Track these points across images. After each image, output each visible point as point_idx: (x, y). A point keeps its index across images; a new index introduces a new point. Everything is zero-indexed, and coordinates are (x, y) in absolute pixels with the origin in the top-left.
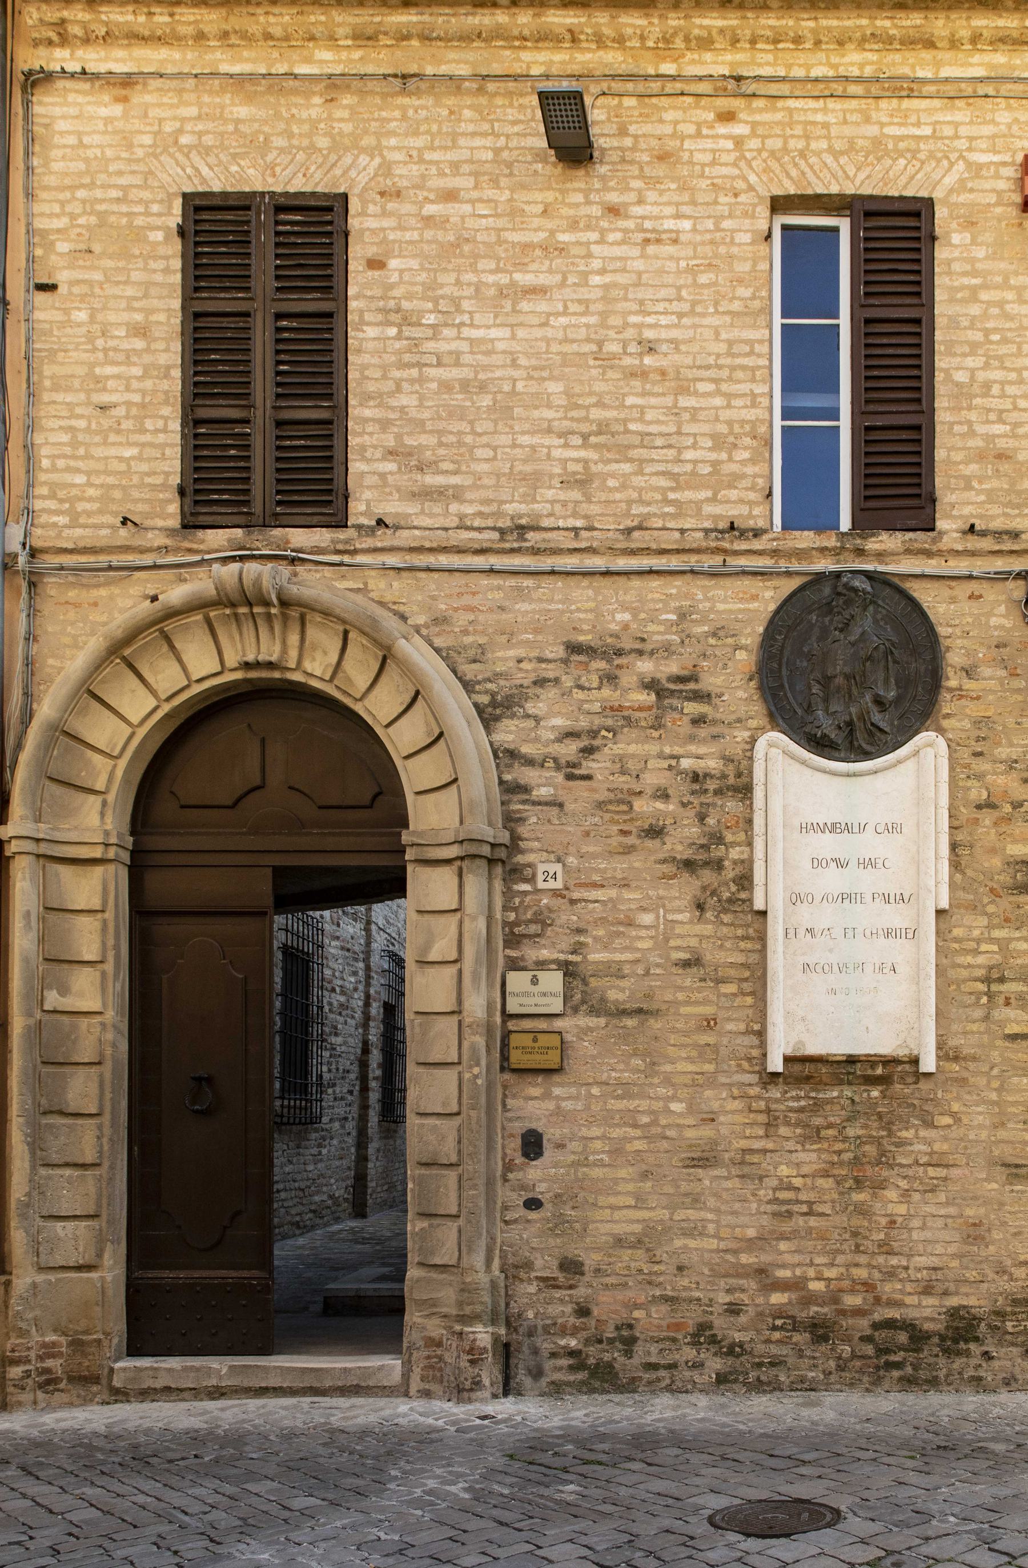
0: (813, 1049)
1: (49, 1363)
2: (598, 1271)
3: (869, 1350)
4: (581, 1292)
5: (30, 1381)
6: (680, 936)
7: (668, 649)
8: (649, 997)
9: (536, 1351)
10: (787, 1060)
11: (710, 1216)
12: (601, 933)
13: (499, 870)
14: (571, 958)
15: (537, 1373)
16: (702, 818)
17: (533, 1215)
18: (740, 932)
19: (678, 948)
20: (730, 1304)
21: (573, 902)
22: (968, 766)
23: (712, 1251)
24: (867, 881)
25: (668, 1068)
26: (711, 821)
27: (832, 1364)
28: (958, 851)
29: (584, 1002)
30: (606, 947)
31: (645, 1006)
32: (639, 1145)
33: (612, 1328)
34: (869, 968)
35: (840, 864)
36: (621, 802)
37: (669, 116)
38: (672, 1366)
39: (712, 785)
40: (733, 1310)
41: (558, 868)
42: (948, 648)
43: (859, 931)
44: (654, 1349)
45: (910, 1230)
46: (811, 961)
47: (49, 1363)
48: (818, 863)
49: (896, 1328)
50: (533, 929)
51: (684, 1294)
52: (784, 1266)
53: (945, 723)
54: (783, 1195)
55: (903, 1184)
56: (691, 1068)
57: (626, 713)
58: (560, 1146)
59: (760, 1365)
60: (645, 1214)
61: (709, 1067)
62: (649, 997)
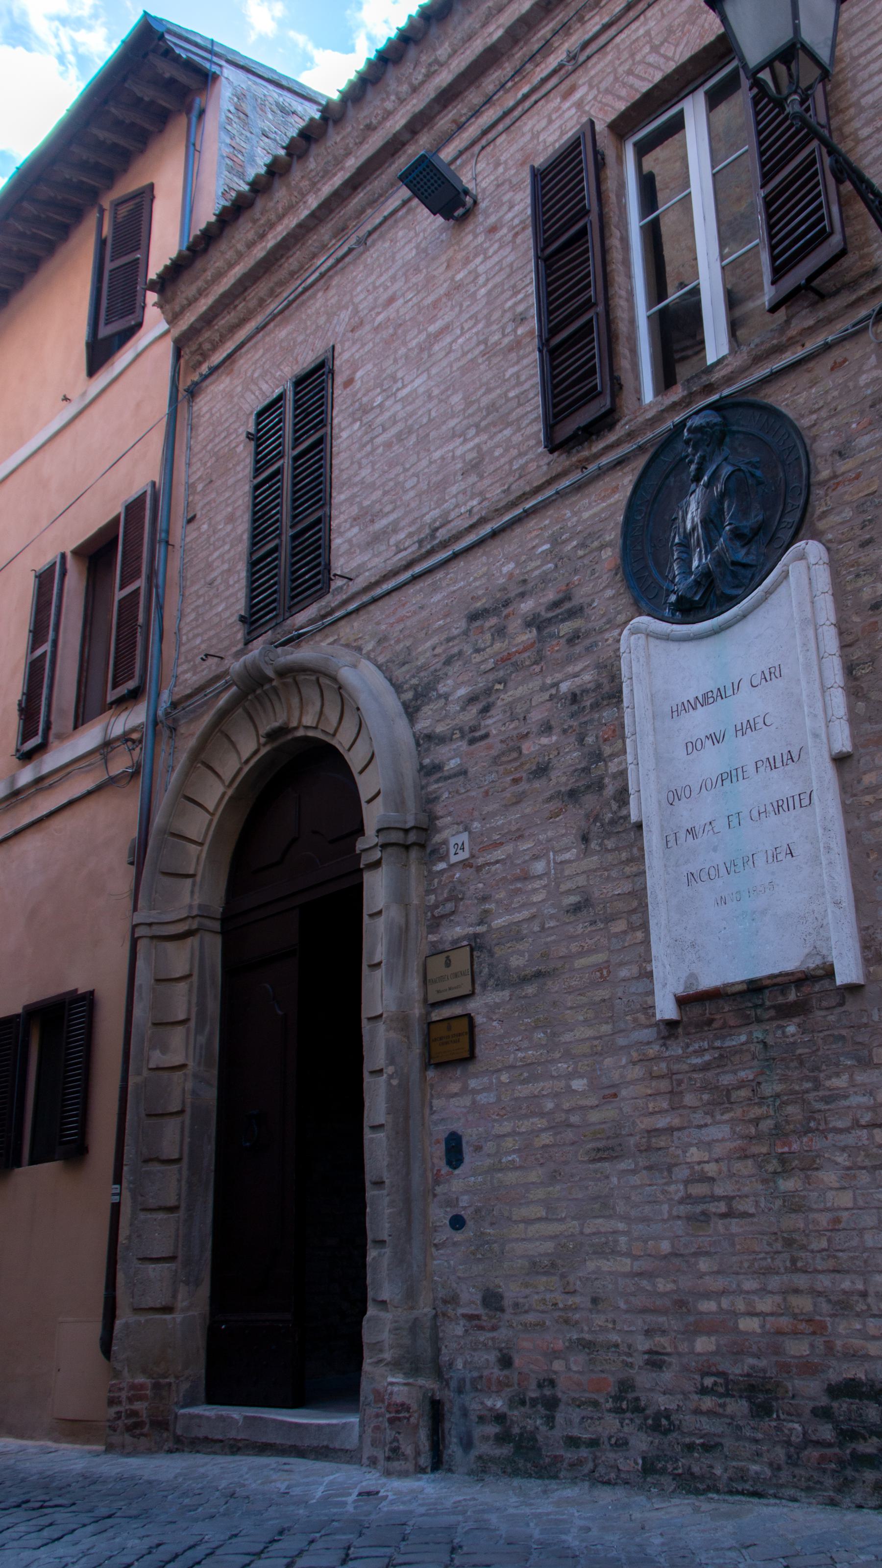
0: (708, 981)
1: (138, 1406)
2: (516, 1305)
3: (826, 1432)
4: (503, 1333)
5: (120, 1423)
6: (570, 877)
7: (545, 579)
8: (545, 956)
9: (465, 1413)
10: (682, 1002)
11: (621, 1226)
12: (502, 895)
13: (414, 854)
14: (480, 929)
15: (467, 1444)
16: (581, 740)
17: (458, 1236)
18: (624, 855)
19: (569, 892)
20: (650, 1352)
21: (479, 869)
22: (856, 563)
23: (626, 1275)
24: (747, 750)
25: (567, 1037)
26: (590, 740)
27: (780, 1453)
28: (858, 673)
29: (491, 975)
30: (508, 910)
31: (542, 968)
32: (546, 1138)
33: (533, 1385)
34: (760, 860)
35: (715, 739)
36: (512, 749)
37: (526, 129)
38: (594, 1443)
39: (588, 702)
40: (655, 1361)
41: (464, 837)
42: (814, 439)
43: (745, 814)
44: (576, 1414)
45: (861, 1231)
46: (693, 868)
47: (138, 1406)
48: (692, 747)
49: (861, 1396)
50: (450, 906)
51: (601, 1338)
52: (707, 1295)
53: (821, 525)
54: (698, 1189)
55: (842, 1159)
56: (590, 1033)
57: (514, 659)
58: (478, 1149)
59: (690, 1447)
60: (554, 1228)
61: (606, 1028)
62: (545, 956)
